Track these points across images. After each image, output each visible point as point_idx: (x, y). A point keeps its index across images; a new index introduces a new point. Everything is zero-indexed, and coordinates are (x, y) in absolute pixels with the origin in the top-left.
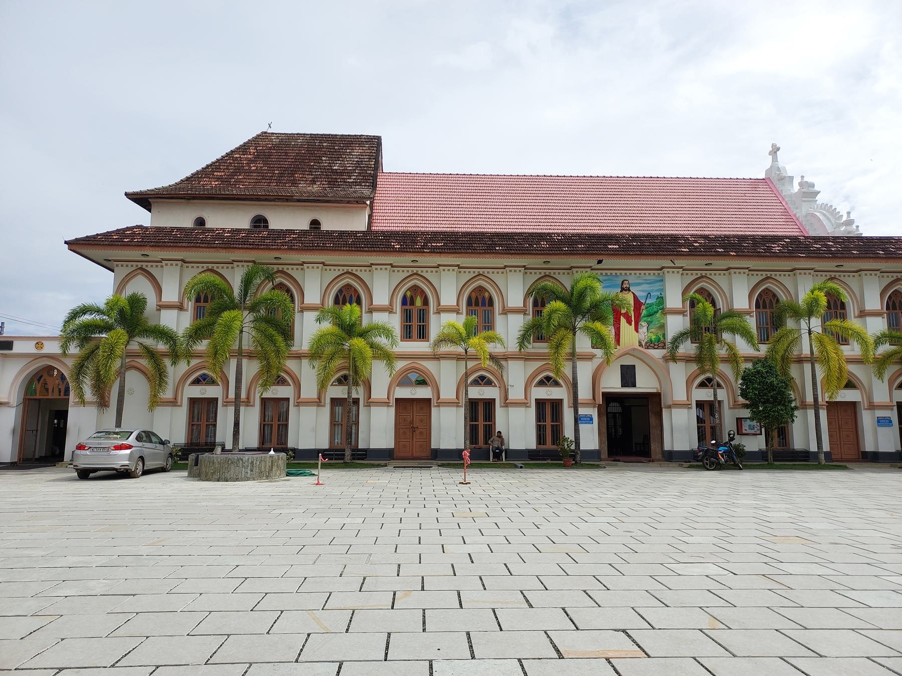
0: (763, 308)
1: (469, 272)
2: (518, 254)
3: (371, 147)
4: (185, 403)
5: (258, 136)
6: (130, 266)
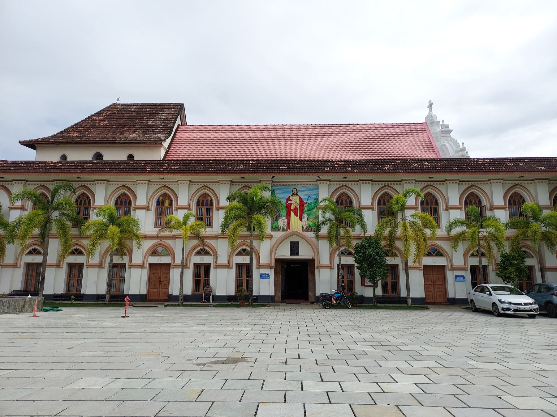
0: (514, 205)
1: (198, 185)
2: (221, 173)
3: (175, 110)
4: (234, 266)
5: (110, 106)
6: (159, 184)
